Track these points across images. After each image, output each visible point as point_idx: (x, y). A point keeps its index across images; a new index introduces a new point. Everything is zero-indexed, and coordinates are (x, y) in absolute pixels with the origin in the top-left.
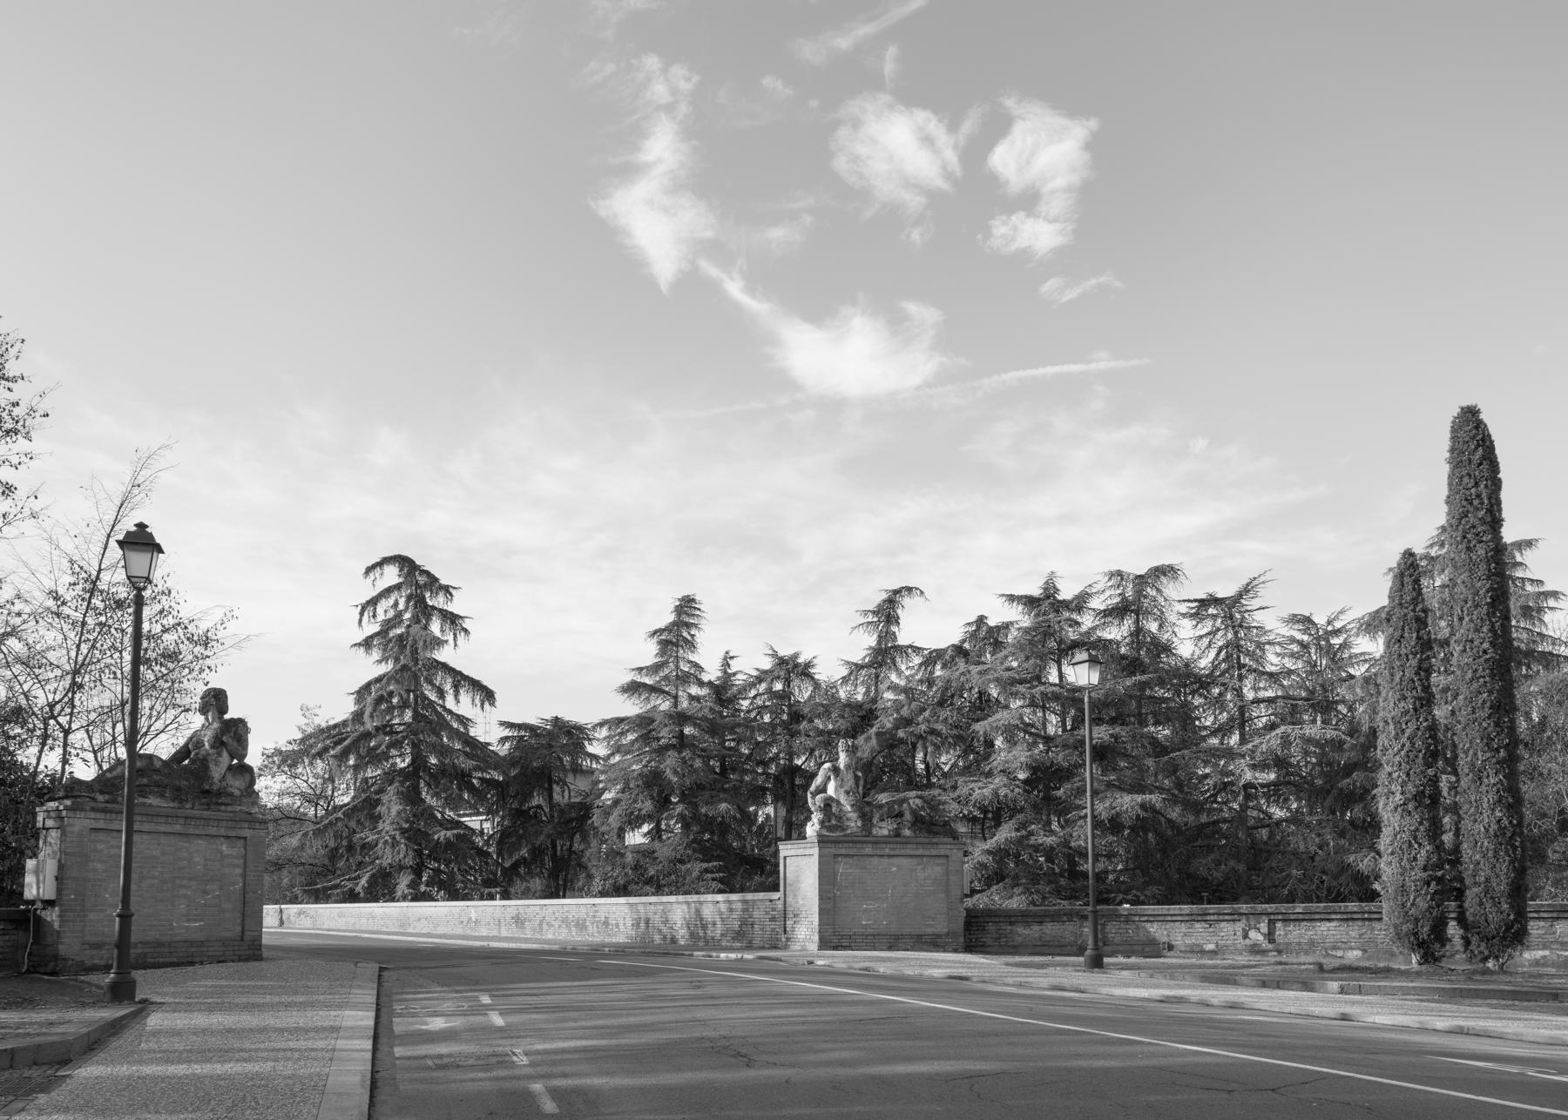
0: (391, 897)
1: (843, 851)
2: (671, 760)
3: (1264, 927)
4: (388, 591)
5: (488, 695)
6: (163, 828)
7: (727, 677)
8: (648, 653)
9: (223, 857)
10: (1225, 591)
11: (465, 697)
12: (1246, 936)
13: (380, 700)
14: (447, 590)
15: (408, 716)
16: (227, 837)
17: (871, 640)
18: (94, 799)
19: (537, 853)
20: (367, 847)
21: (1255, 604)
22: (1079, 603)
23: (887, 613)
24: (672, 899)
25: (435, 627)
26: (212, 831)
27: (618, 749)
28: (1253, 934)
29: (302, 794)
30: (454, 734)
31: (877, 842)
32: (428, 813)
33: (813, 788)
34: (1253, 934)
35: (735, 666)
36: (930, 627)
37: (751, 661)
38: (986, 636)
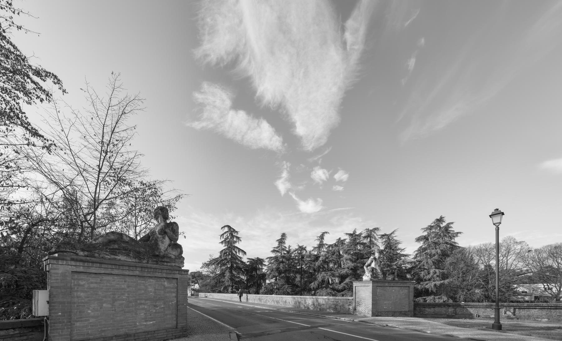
0: (227, 292)
2: (281, 265)
3: (512, 310)
4: (226, 232)
5: (245, 253)
6: (127, 273)
7: (290, 250)
8: (276, 244)
9: (165, 288)
10: (388, 233)
11: (241, 253)
12: (505, 313)
13: (225, 253)
14: (237, 232)
15: (230, 257)
16: (167, 278)
17: (318, 243)
18: (77, 254)
19: (254, 283)
20: (223, 282)
22: (360, 235)
23: (322, 237)
24: (308, 297)
25: (235, 239)
26: (159, 275)
27: (270, 263)
28: (508, 313)
30: (239, 260)
31: (389, 282)
32: (234, 275)
33: (366, 264)
34: (508, 313)
35: (291, 248)
36: (330, 240)
37: (294, 247)
38: (340, 242)
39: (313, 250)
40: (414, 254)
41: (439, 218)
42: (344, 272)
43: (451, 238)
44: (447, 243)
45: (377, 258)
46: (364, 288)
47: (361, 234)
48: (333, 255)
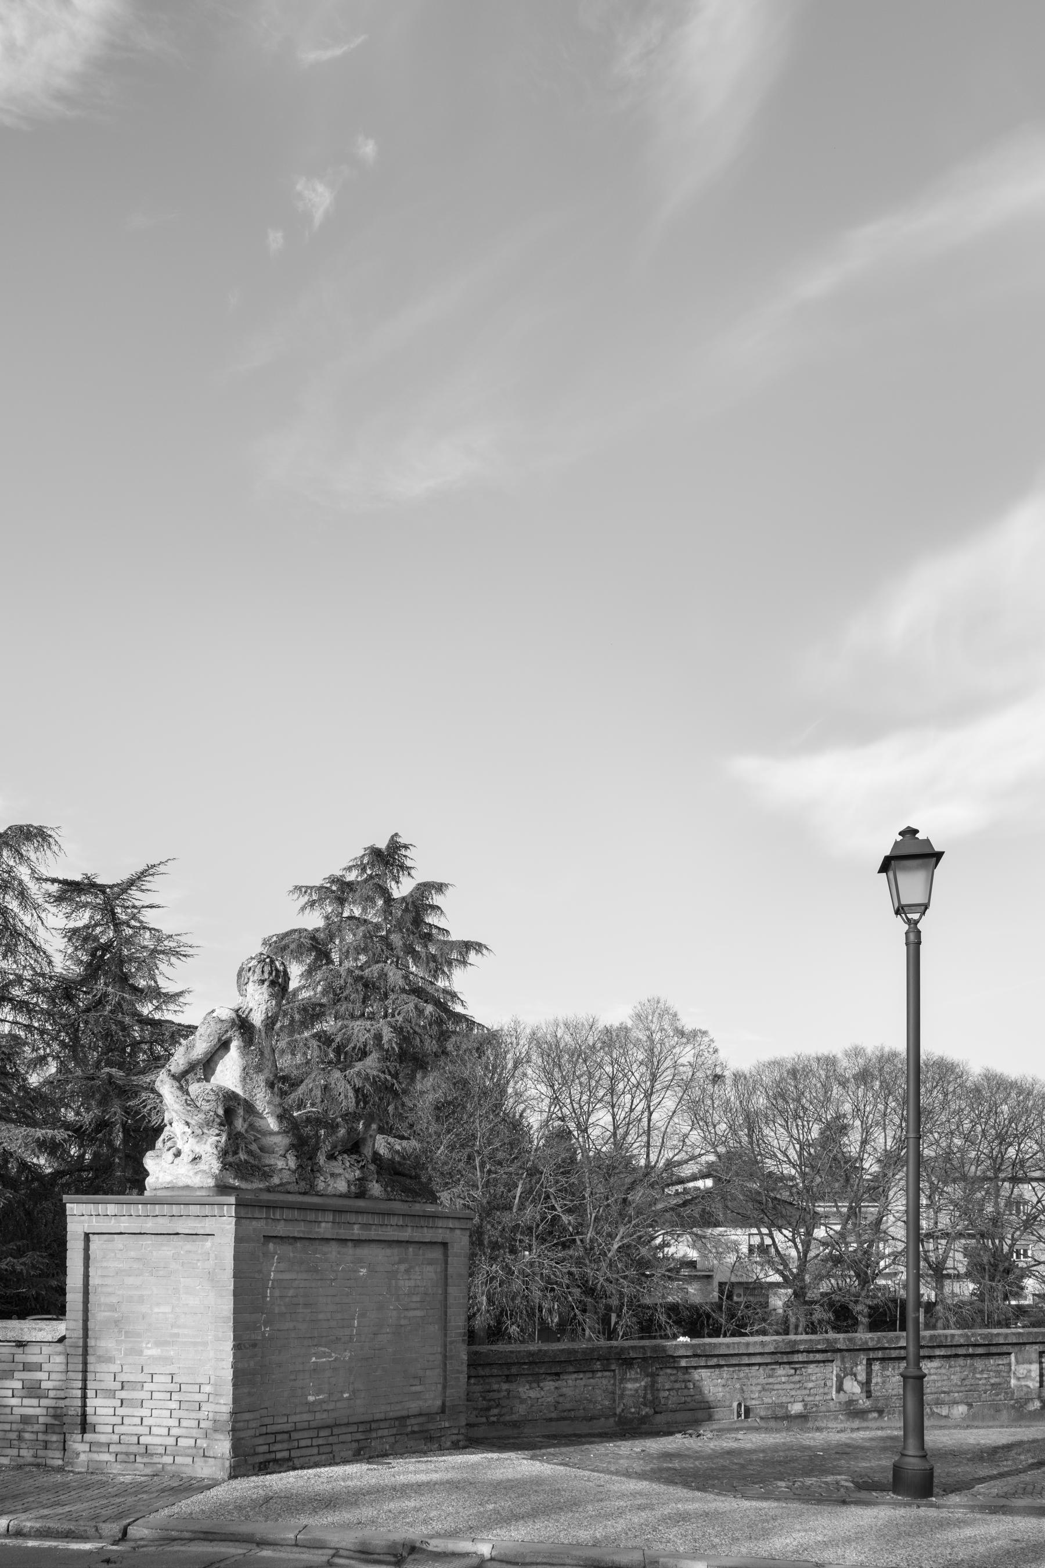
1: (281, 1229)
12: (840, 1389)
21: (144, 899)
33: (179, 1060)
41: (382, 844)
43: (437, 971)
44: (417, 992)
45: (257, 1019)
46: (167, 1250)
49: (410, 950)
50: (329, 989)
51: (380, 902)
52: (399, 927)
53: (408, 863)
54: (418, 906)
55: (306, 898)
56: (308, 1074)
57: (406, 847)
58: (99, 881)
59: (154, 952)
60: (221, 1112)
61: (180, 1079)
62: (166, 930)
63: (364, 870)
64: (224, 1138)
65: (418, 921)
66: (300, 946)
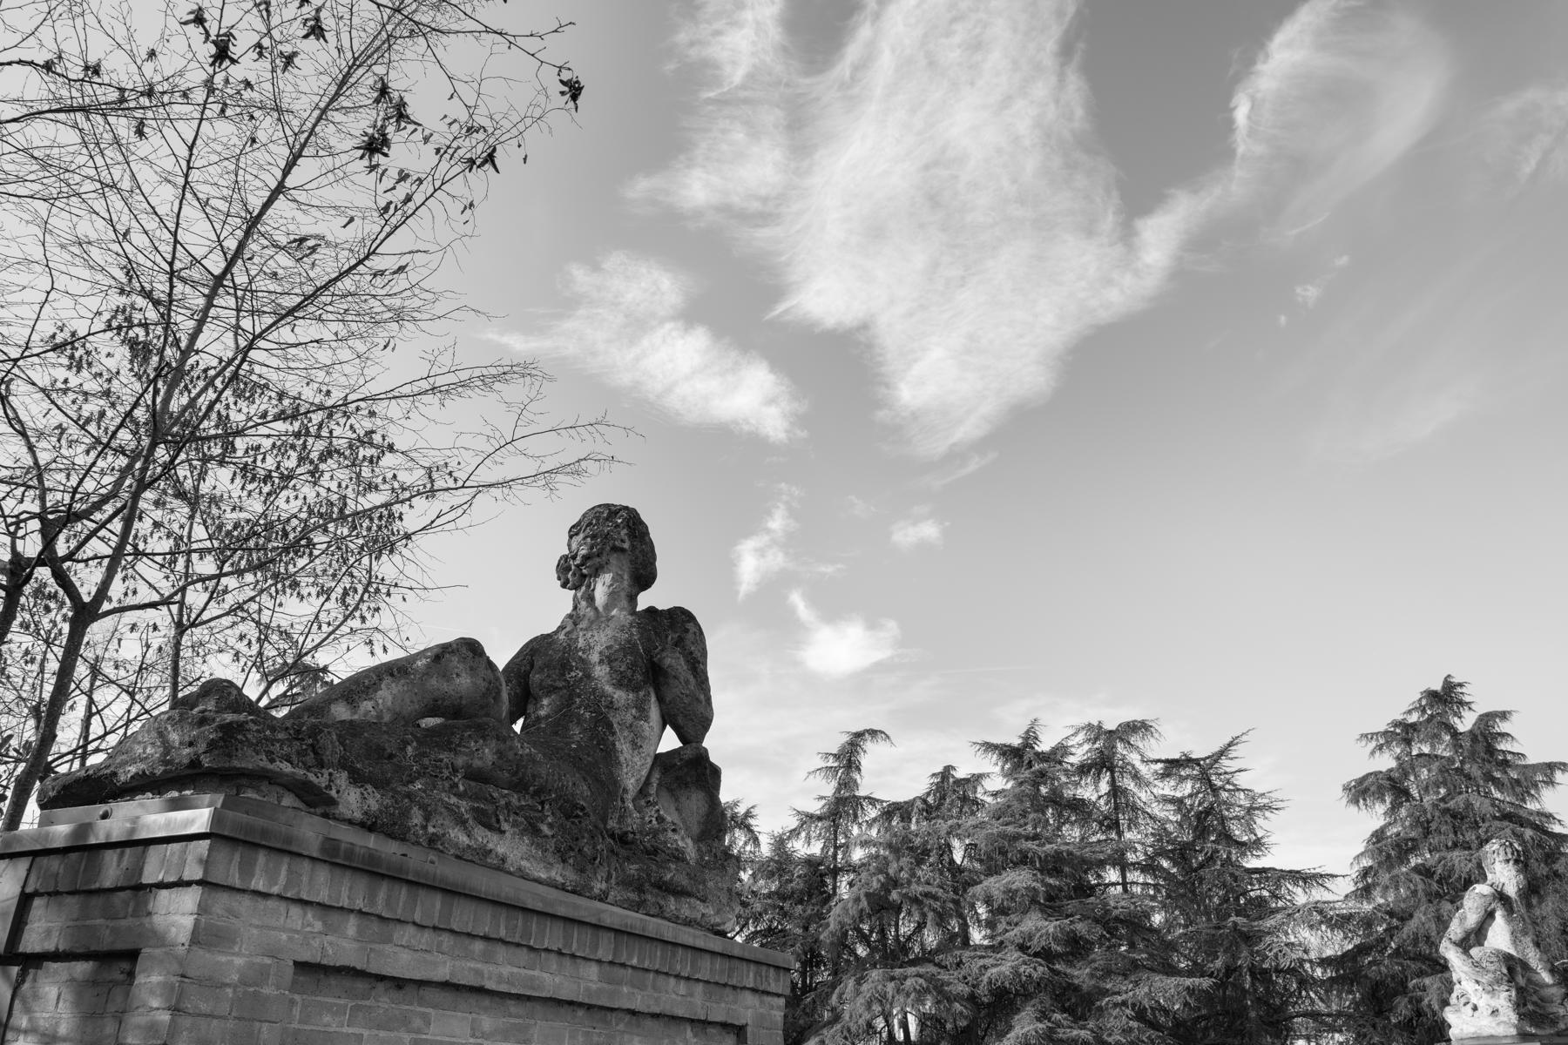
10: (1201, 750)
17: (829, 788)
22: (1057, 755)
23: (848, 759)
29: (1033, 901)
33: (1456, 929)
36: (895, 776)
38: (952, 791)
39: (794, 833)
40: (1354, 872)
42: (1006, 968)
45: (1511, 890)
47: (1060, 751)
48: (920, 862)
49: (1489, 778)
50: (1417, 822)
51: (1448, 738)
52: (1473, 756)
53: (1467, 699)
54: (1486, 737)
55: (1373, 744)
56: (1416, 907)
57: (1461, 685)
58: (1194, 756)
59: (1250, 810)
60: (1505, 971)
61: (1465, 944)
62: (1258, 790)
63: (1424, 711)
64: (1514, 993)
65: (1491, 751)
66: (1380, 787)
